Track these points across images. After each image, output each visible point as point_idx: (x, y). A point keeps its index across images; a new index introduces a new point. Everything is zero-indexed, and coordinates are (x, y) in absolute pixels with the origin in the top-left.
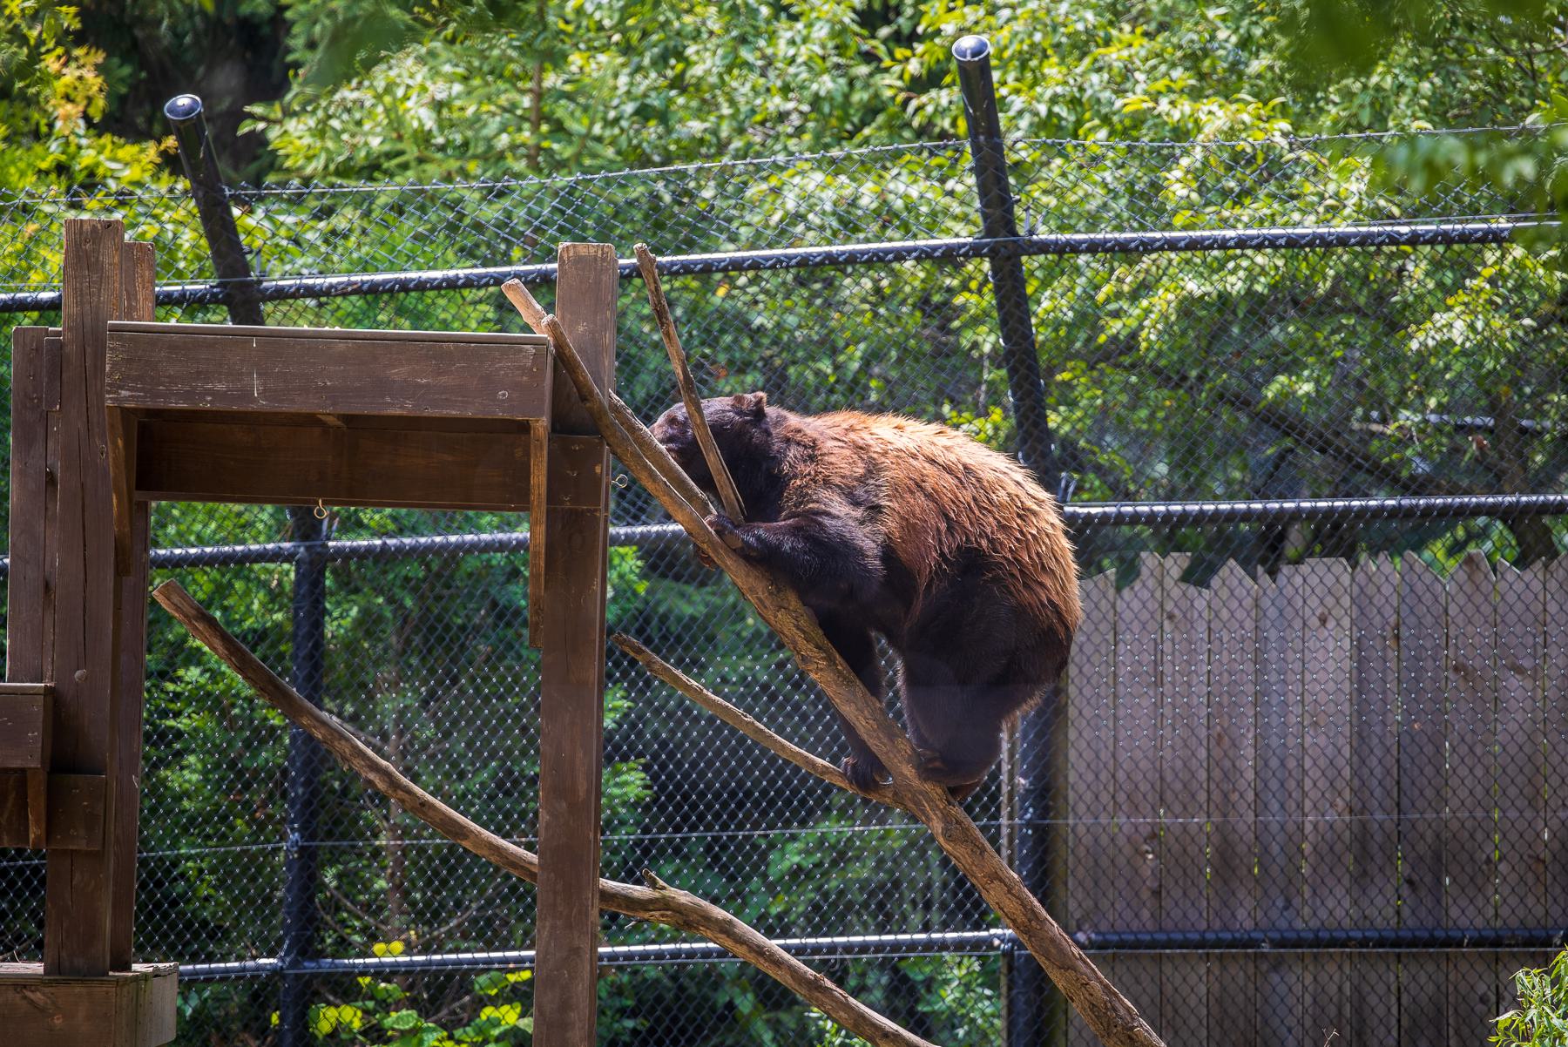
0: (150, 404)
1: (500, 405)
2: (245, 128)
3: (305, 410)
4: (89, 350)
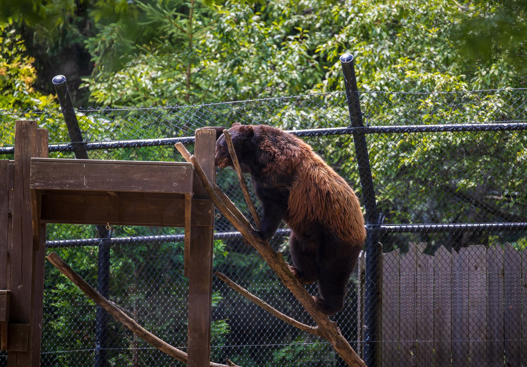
0: (46, 188)
1: (175, 188)
2: (82, 86)
3: (102, 190)
4: (24, 168)
